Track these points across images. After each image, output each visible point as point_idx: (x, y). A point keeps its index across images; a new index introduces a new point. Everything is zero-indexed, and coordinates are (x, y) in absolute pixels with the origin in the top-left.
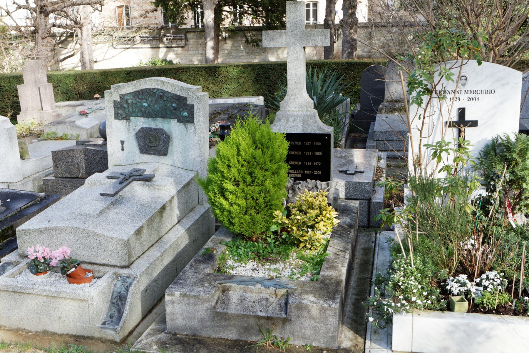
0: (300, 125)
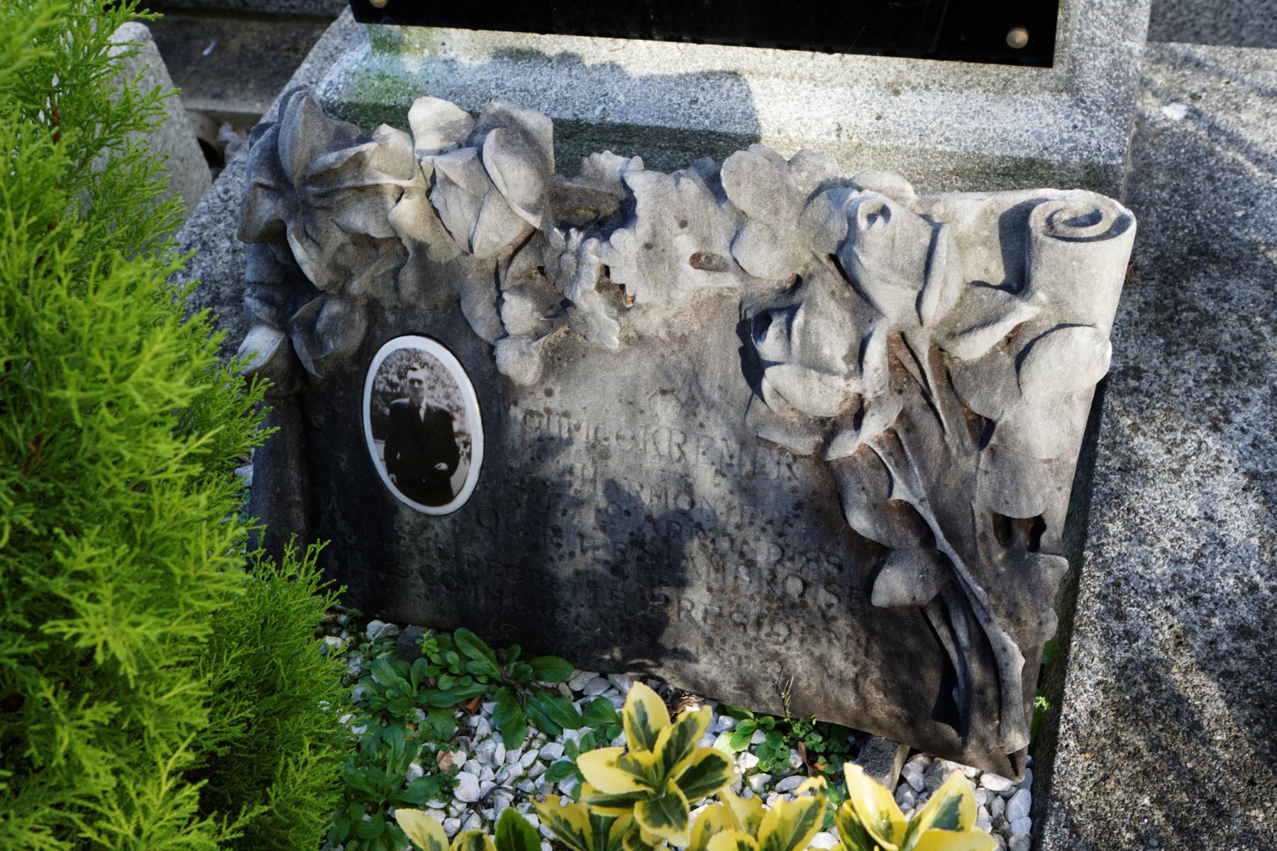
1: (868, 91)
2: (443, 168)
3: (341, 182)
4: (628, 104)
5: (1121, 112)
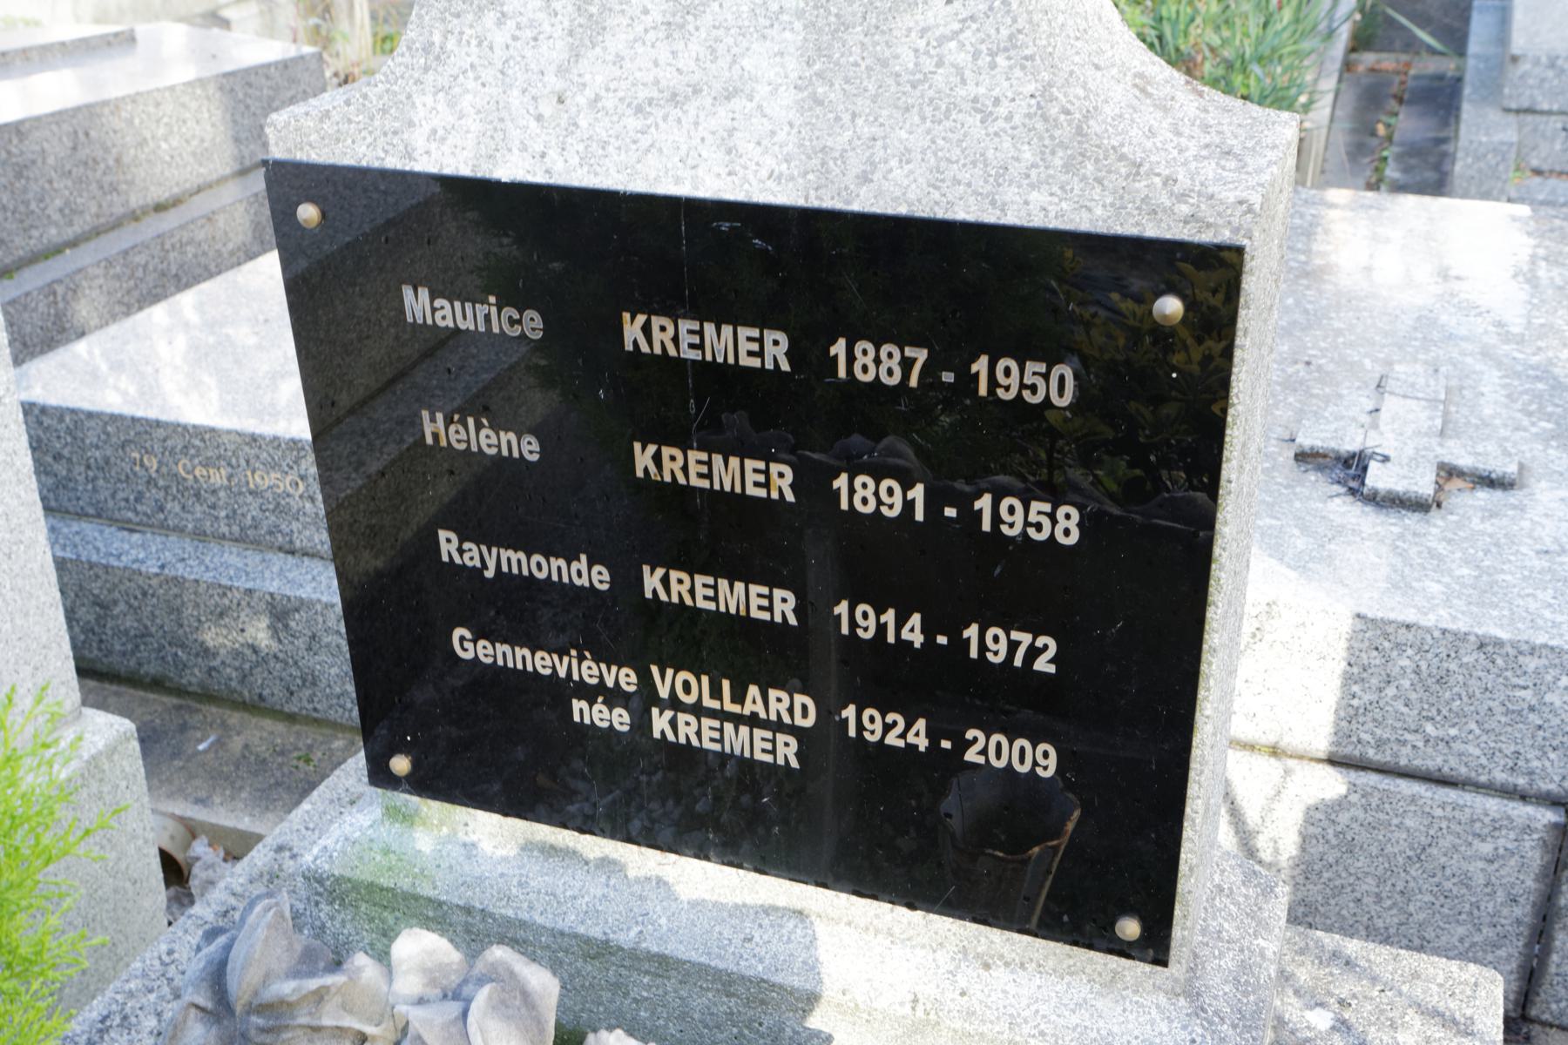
0: (772, 64)
1: (953, 959)
2: (417, 1025)
3: (293, 1018)
4: (670, 930)
5: (1248, 1029)
